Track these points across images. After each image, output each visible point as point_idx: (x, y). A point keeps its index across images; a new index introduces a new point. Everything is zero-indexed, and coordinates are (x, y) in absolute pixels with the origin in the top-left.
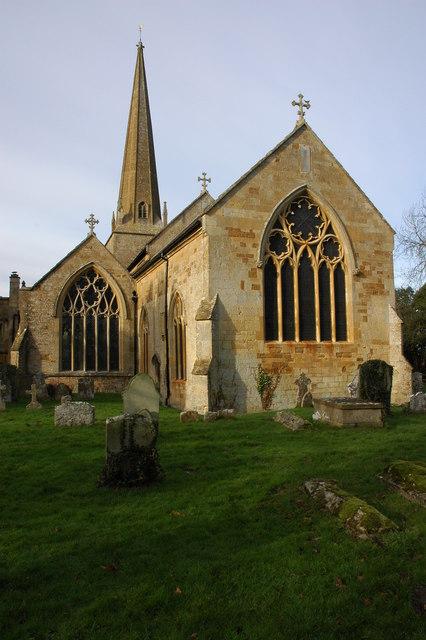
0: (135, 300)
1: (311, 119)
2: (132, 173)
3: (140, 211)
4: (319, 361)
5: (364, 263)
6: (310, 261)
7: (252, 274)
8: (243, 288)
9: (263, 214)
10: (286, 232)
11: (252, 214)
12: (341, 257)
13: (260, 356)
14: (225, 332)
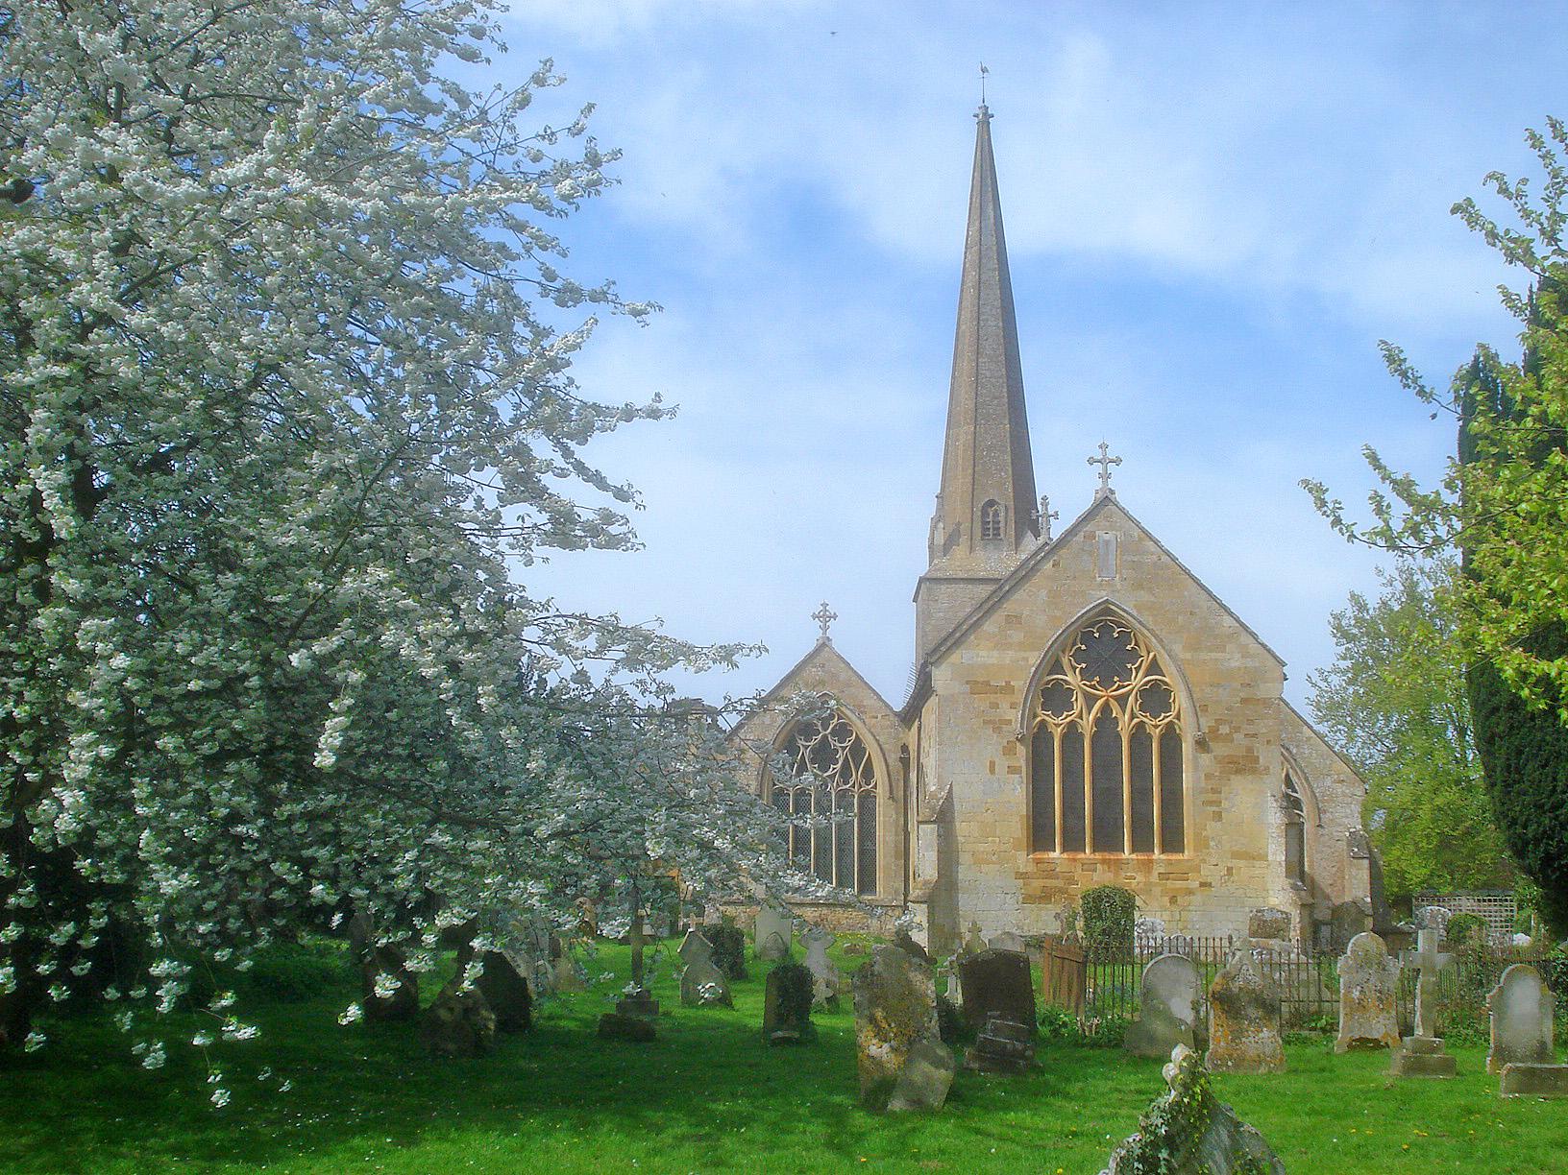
2: (965, 431)
3: (985, 523)
7: (1008, 750)
8: (992, 771)
10: (1073, 679)
11: (1009, 656)
13: (1020, 875)
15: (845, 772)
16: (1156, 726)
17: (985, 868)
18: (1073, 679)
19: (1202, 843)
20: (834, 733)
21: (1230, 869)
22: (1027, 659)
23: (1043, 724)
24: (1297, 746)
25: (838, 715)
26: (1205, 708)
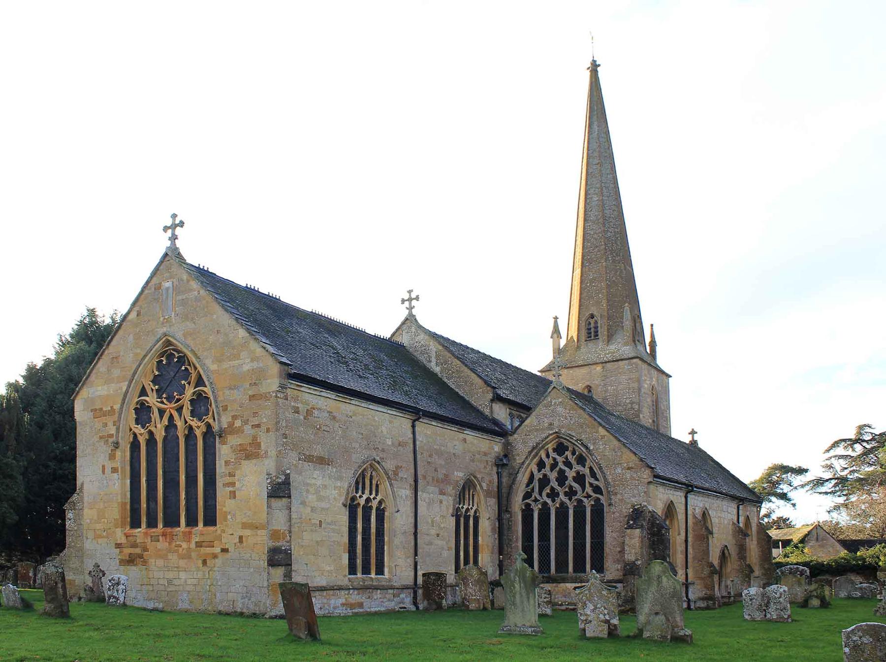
5: (235, 417)
10: (152, 399)
13: (118, 546)
14: (88, 521)
17: (100, 541)
18: (152, 399)
21: (241, 538)
24: (594, 444)
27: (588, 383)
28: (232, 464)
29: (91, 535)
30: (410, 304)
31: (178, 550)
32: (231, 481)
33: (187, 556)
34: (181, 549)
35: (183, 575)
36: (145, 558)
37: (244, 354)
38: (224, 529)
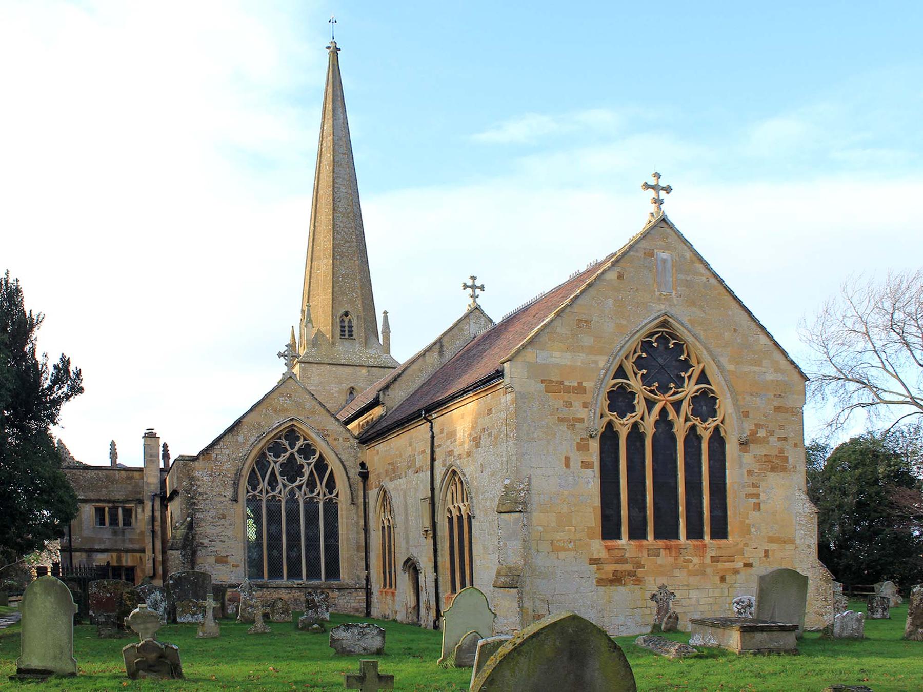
0: (365, 476)
1: (673, 209)
2: (325, 265)
4: (682, 567)
5: (758, 426)
6: (670, 424)
7: (582, 447)
8: (567, 465)
9: (598, 357)
10: (635, 384)
11: (580, 359)
12: (719, 418)
13: (594, 561)
14: (541, 529)
15: (312, 485)
16: (706, 429)
17: (562, 555)
18: (635, 384)
19: (746, 530)
20: (300, 451)
21: (766, 552)
22: (596, 362)
23: (610, 425)
25: (303, 436)
26: (746, 415)
27: (352, 385)
28: (756, 474)
29: (545, 547)
30: (474, 291)
31: (688, 566)
32: (755, 492)
33: (701, 572)
34: (691, 565)
35: (694, 594)
36: (638, 575)
37: (765, 362)
38: (747, 542)
